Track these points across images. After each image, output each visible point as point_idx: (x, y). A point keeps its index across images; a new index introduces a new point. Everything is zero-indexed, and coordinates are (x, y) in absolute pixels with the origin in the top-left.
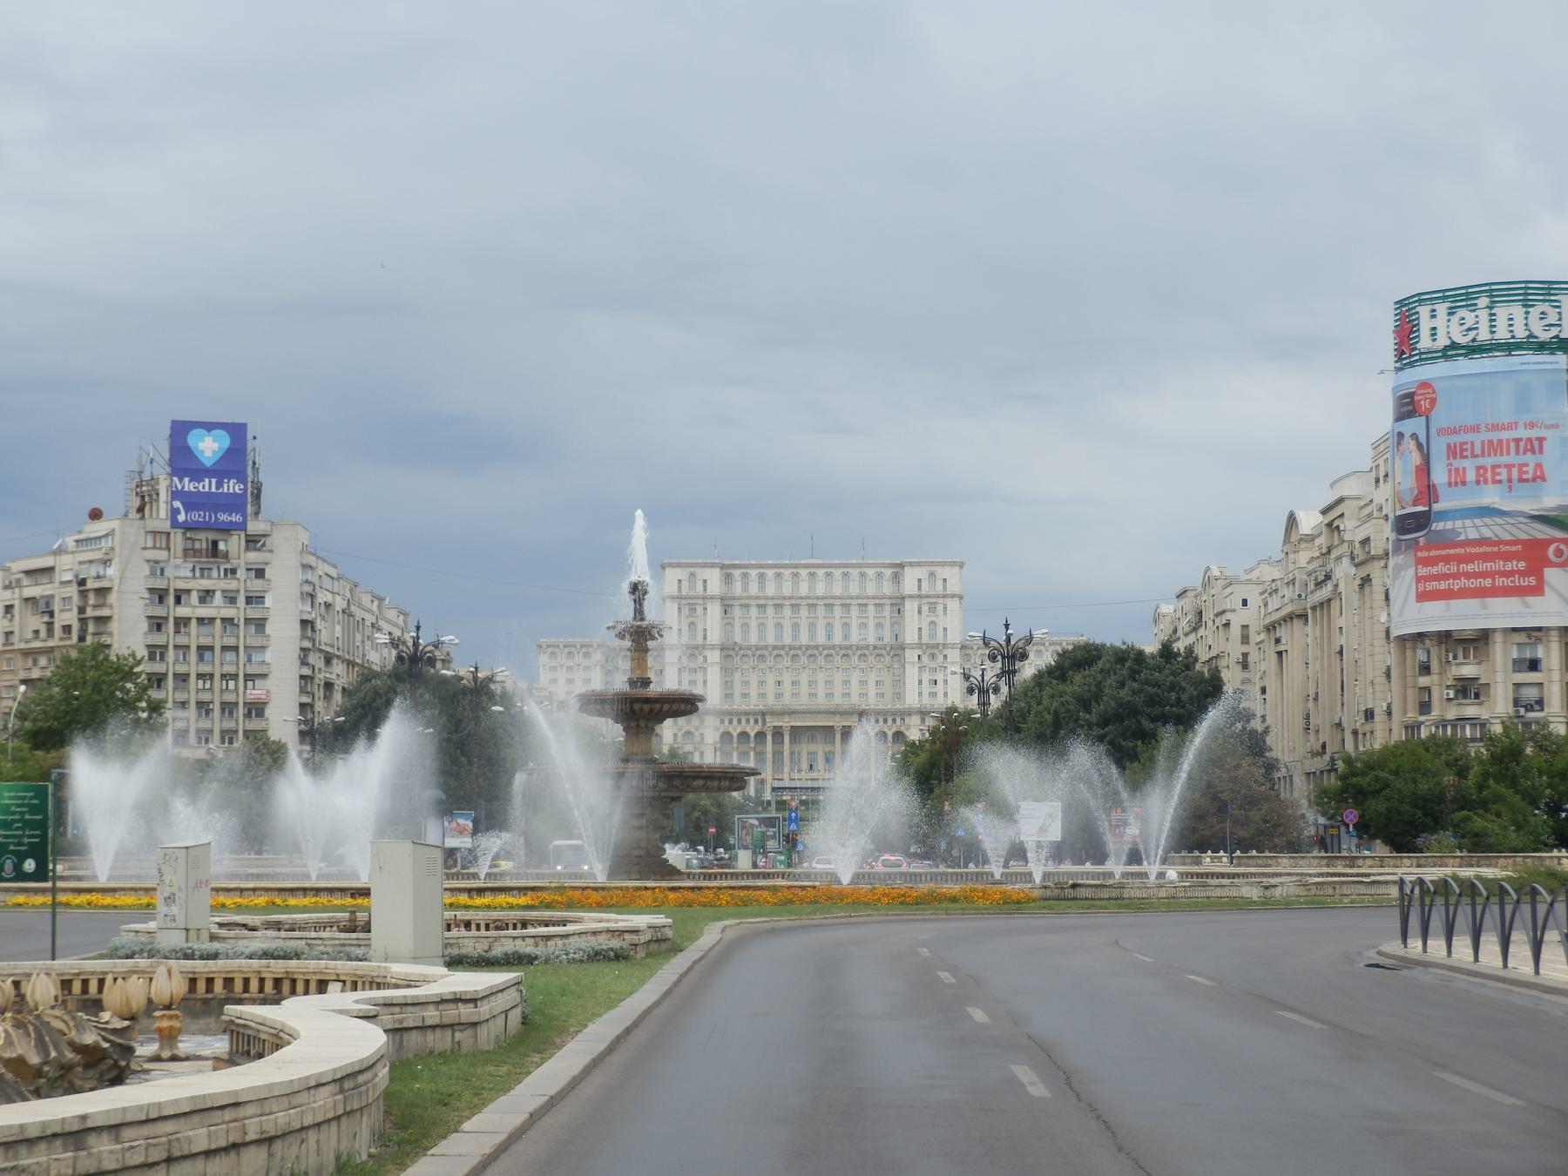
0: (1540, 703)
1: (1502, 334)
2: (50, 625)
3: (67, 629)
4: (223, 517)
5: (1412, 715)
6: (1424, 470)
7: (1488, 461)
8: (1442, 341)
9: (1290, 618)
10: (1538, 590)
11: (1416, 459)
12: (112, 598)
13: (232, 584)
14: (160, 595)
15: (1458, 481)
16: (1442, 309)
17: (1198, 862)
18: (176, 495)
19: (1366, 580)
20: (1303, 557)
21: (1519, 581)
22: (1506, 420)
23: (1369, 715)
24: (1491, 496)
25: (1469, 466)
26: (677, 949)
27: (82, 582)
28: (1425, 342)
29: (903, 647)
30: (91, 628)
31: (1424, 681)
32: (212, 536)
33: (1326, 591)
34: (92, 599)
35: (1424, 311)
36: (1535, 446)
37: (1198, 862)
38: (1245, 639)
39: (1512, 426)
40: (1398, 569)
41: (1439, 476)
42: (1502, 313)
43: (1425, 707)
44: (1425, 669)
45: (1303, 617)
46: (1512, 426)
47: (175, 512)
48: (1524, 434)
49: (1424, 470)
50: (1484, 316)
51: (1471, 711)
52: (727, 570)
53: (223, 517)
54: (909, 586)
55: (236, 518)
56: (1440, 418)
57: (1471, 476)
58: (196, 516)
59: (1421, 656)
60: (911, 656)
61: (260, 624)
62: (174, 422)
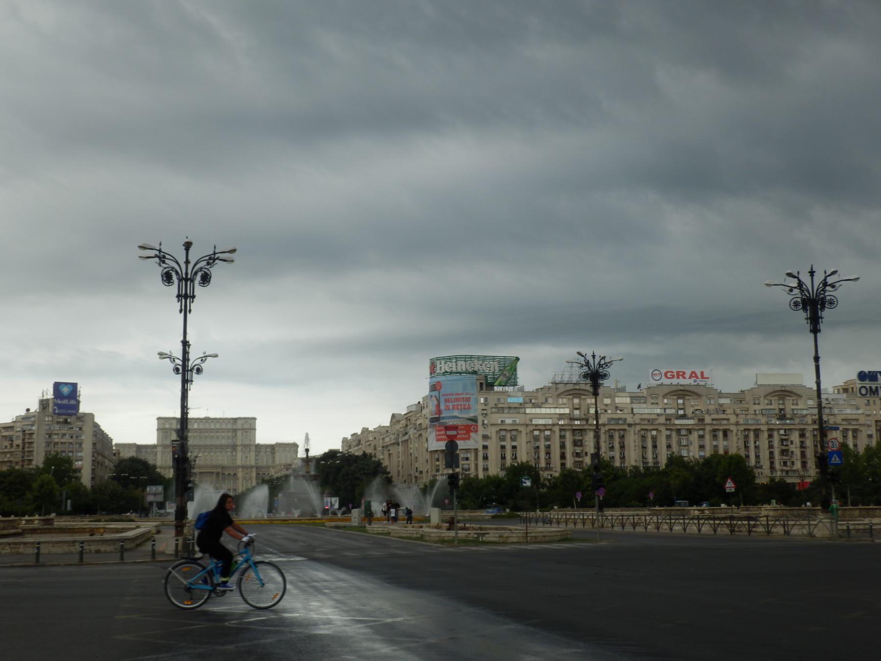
0: (469, 469)
1: (459, 370)
2: (11, 445)
3: (18, 446)
4: (70, 411)
6: (438, 405)
7: (456, 403)
8: (443, 371)
9: (393, 444)
10: (468, 438)
11: (436, 402)
12: (34, 436)
13: (71, 432)
14: (50, 435)
15: (447, 408)
16: (443, 362)
18: (55, 404)
19: (421, 435)
20: (398, 427)
21: (464, 436)
22: (460, 392)
23: (421, 472)
24: (456, 413)
25: (451, 405)
27: (24, 431)
28: (438, 371)
29: (236, 446)
30: (27, 445)
31: (437, 463)
32: (66, 417)
33: (406, 437)
34: (27, 437)
35: (438, 362)
36: (468, 400)
38: (375, 449)
39: (462, 394)
40: (431, 432)
41: (442, 407)
42: (459, 363)
43: (438, 470)
44: (438, 460)
45: (398, 444)
46: (462, 394)
47: (55, 410)
48: (464, 396)
49: (438, 405)
50: (454, 364)
53: (70, 411)
55: (74, 412)
56: (442, 391)
57: (451, 407)
58: (62, 411)
59: (436, 456)
60: (239, 449)
61: (80, 444)
62: (255, 419)
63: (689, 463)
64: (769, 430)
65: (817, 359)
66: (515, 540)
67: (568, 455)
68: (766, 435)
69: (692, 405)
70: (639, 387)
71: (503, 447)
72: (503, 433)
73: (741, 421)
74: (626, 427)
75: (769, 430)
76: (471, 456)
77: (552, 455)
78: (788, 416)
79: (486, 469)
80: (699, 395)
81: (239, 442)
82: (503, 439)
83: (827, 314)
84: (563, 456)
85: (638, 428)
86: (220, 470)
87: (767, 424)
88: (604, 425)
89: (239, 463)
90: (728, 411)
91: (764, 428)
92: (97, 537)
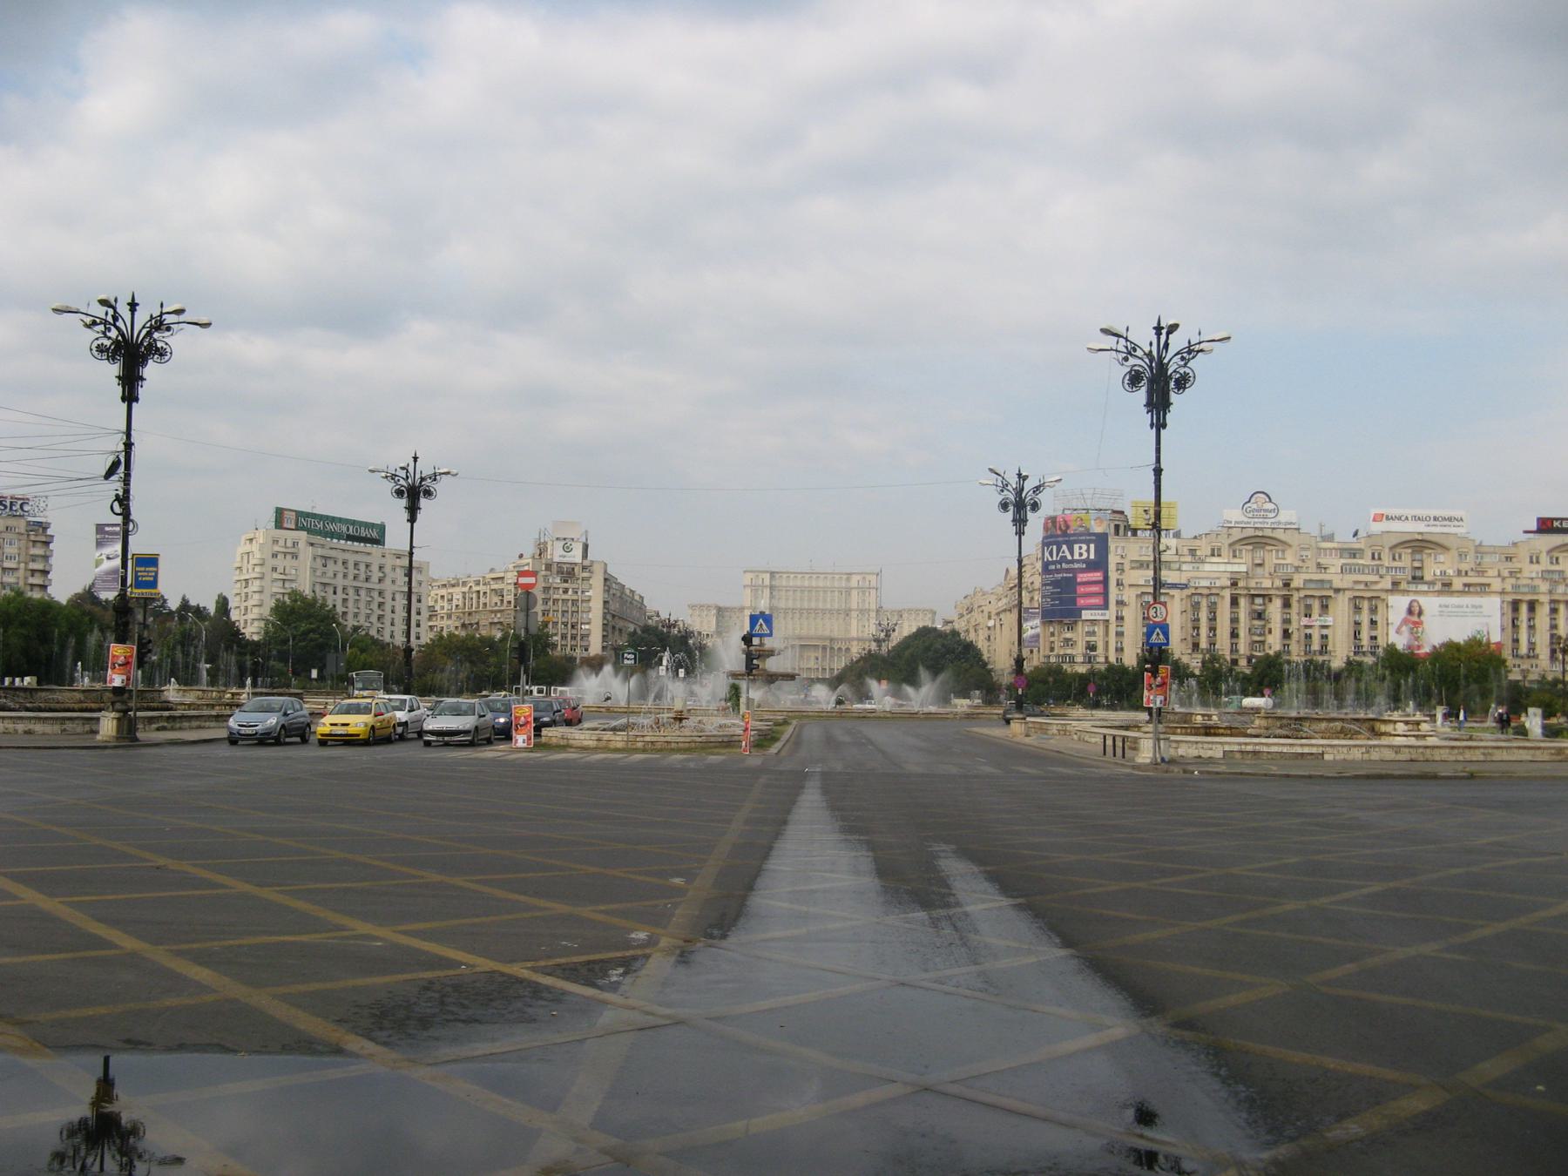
5: (1048, 652)
17: (1372, 728)
26: (775, 740)
37: (1372, 728)
43: (1052, 649)
44: (1052, 634)
51: (1069, 651)
52: (772, 574)
54: (854, 583)
60: (854, 614)
63: (266, 633)
64: (1552, 601)
65: (1158, 472)
66: (620, 745)
67: (1242, 633)
68: (1546, 609)
69: (1271, 558)
70: (1356, 534)
71: (1357, 624)
72: (1196, 598)
73: (1509, 589)
74: (1331, 593)
75: (1552, 601)
76: (1100, 630)
77: (1218, 632)
78: (1427, 578)
79: (1120, 650)
80: (1445, 548)
81: (854, 606)
82: (1357, 609)
83: (151, 370)
84: (1234, 634)
85: (1349, 594)
86: (827, 643)
87: (1550, 592)
88: (1298, 589)
89: (854, 634)
90: (1491, 573)
91: (1544, 599)
92: (1338, 725)
